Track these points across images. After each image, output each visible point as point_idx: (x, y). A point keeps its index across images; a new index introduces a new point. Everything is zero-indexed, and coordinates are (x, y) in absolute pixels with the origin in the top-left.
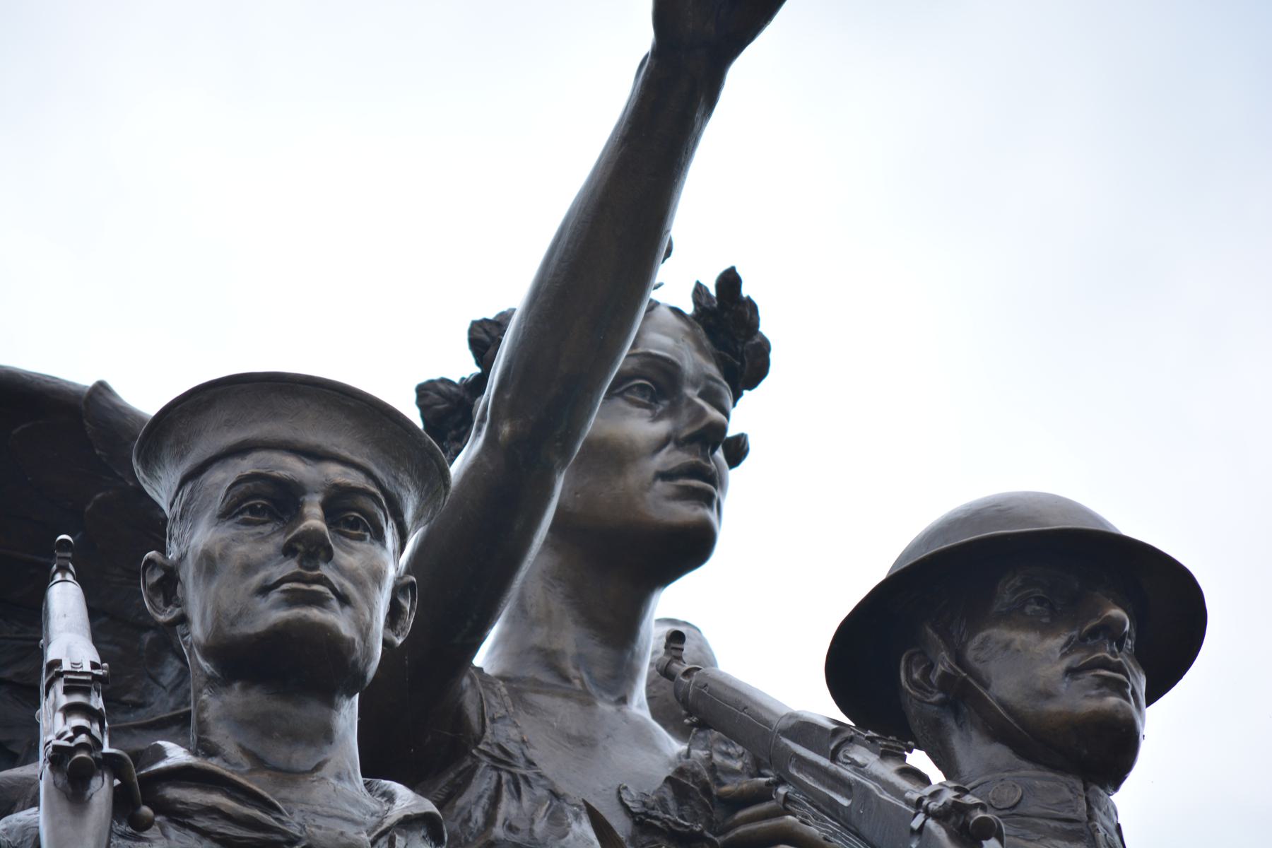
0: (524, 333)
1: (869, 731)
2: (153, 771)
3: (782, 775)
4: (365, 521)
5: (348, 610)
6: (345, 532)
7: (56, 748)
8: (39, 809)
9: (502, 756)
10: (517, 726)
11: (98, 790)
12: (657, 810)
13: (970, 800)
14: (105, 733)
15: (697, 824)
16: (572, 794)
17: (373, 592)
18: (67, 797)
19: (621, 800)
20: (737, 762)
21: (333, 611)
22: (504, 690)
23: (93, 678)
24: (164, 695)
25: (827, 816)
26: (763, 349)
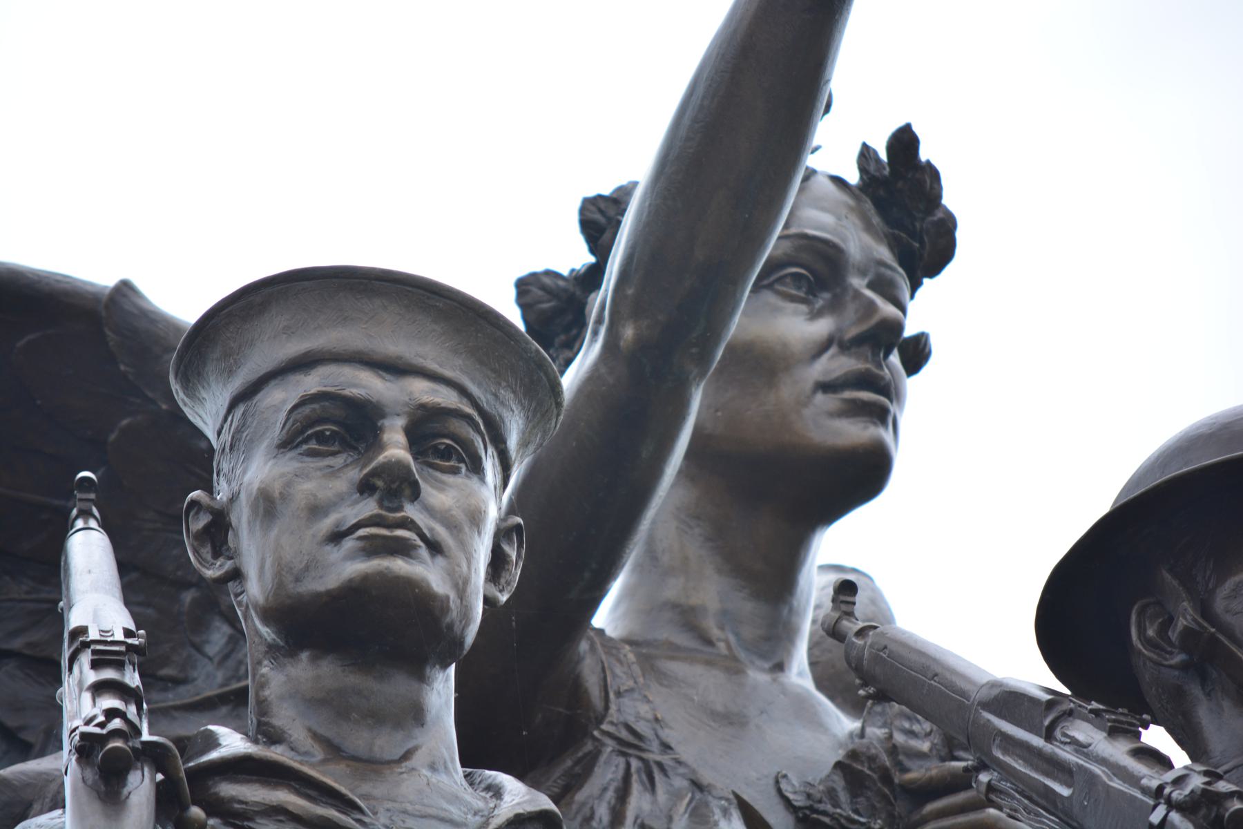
0: (649, 212)
1: (1093, 702)
2: (203, 762)
3: (983, 758)
4: (459, 448)
5: (440, 560)
6: (434, 463)
7: (84, 736)
8: (64, 812)
9: (631, 739)
10: (649, 701)
11: (136, 788)
12: (826, 803)
13: (1224, 787)
14: (144, 716)
15: (876, 820)
16: (719, 785)
17: (471, 538)
18: (99, 797)
19: (779, 791)
20: (924, 742)
21: (422, 562)
22: (631, 657)
23: (126, 648)
24: (210, 668)
25: (1041, 808)
26: (947, 227)
